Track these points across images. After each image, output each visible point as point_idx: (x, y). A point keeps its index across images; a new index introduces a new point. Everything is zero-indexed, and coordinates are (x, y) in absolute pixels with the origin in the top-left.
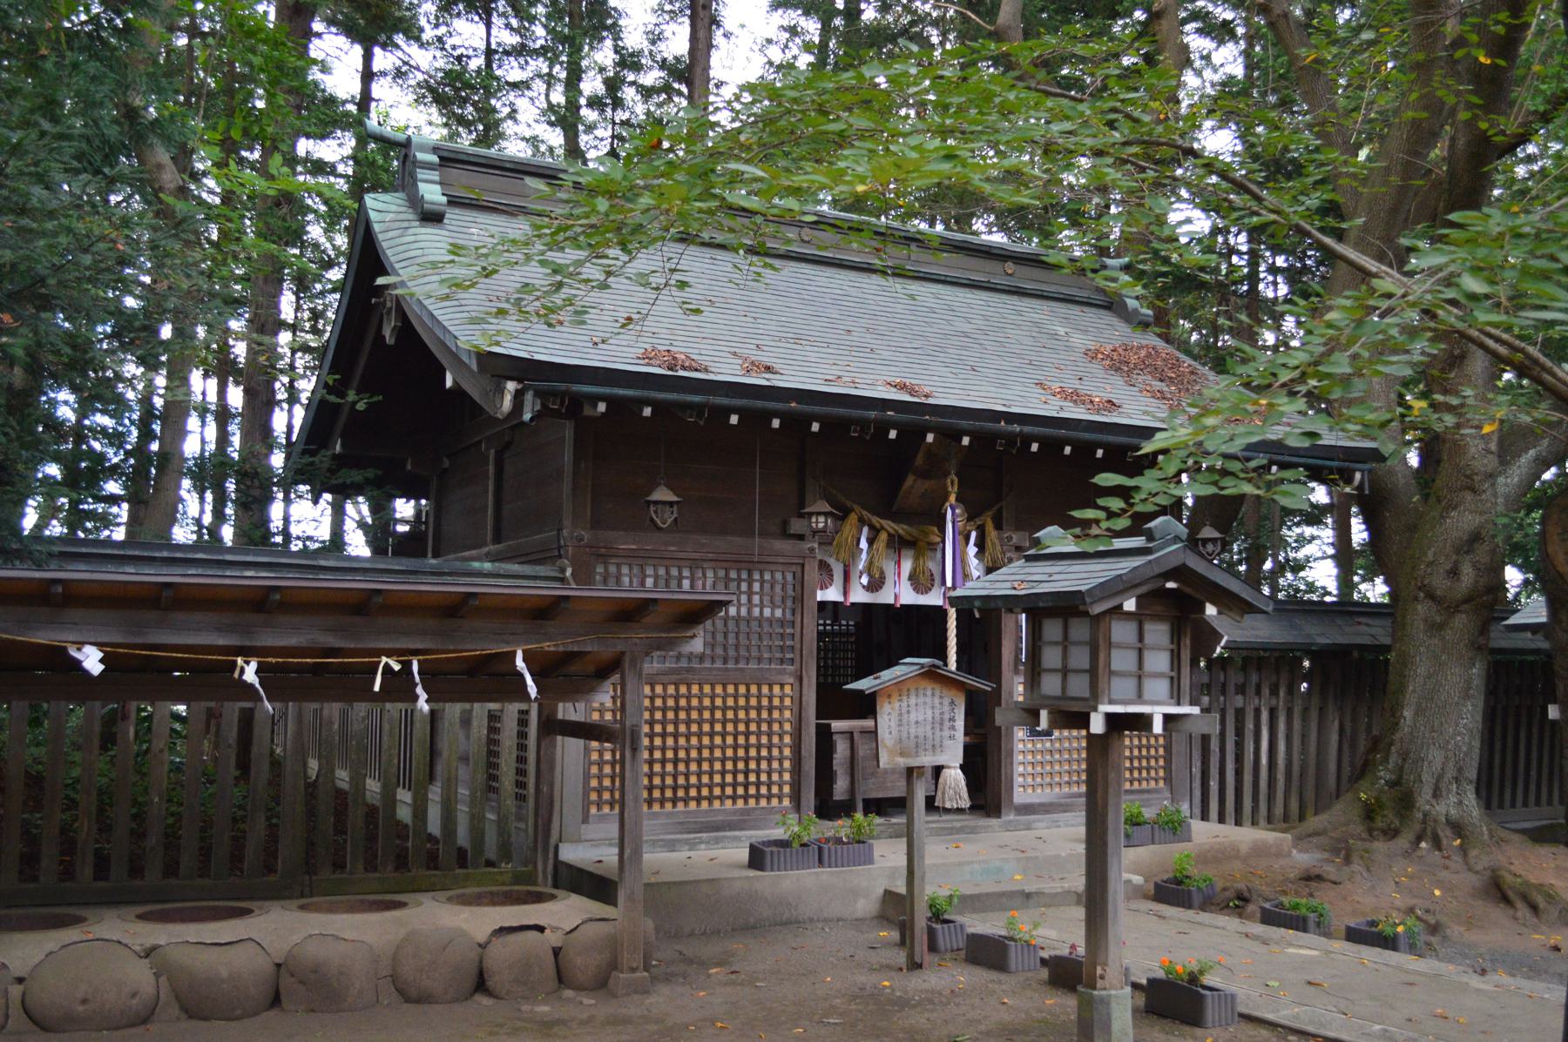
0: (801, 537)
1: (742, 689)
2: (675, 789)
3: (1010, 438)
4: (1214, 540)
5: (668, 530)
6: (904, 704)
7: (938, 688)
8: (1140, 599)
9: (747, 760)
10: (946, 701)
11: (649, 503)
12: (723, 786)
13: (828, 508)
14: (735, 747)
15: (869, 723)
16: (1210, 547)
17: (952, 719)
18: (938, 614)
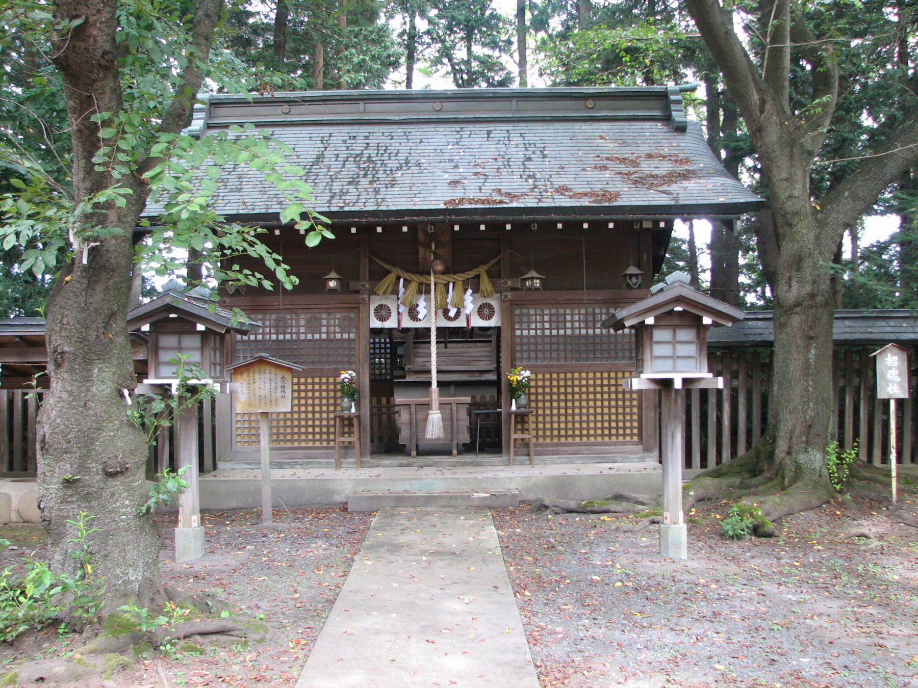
0: (357, 292)
1: (605, 375)
2: (566, 429)
3: (542, 224)
4: (636, 275)
5: (232, 295)
6: (251, 378)
7: (273, 371)
8: (656, 318)
9: (610, 414)
10: (279, 376)
11: (626, 275)
12: (595, 429)
13: (337, 276)
14: (602, 407)
15: (893, 405)
16: (634, 280)
17: (283, 387)
18: (429, 330)
